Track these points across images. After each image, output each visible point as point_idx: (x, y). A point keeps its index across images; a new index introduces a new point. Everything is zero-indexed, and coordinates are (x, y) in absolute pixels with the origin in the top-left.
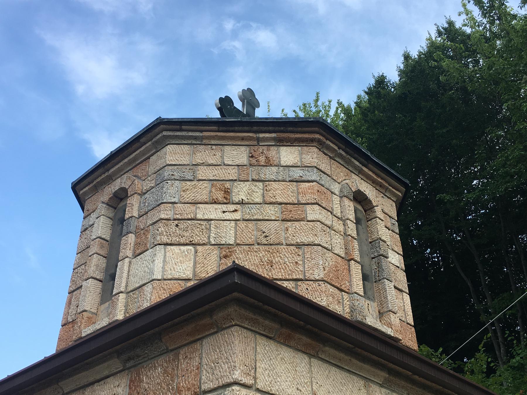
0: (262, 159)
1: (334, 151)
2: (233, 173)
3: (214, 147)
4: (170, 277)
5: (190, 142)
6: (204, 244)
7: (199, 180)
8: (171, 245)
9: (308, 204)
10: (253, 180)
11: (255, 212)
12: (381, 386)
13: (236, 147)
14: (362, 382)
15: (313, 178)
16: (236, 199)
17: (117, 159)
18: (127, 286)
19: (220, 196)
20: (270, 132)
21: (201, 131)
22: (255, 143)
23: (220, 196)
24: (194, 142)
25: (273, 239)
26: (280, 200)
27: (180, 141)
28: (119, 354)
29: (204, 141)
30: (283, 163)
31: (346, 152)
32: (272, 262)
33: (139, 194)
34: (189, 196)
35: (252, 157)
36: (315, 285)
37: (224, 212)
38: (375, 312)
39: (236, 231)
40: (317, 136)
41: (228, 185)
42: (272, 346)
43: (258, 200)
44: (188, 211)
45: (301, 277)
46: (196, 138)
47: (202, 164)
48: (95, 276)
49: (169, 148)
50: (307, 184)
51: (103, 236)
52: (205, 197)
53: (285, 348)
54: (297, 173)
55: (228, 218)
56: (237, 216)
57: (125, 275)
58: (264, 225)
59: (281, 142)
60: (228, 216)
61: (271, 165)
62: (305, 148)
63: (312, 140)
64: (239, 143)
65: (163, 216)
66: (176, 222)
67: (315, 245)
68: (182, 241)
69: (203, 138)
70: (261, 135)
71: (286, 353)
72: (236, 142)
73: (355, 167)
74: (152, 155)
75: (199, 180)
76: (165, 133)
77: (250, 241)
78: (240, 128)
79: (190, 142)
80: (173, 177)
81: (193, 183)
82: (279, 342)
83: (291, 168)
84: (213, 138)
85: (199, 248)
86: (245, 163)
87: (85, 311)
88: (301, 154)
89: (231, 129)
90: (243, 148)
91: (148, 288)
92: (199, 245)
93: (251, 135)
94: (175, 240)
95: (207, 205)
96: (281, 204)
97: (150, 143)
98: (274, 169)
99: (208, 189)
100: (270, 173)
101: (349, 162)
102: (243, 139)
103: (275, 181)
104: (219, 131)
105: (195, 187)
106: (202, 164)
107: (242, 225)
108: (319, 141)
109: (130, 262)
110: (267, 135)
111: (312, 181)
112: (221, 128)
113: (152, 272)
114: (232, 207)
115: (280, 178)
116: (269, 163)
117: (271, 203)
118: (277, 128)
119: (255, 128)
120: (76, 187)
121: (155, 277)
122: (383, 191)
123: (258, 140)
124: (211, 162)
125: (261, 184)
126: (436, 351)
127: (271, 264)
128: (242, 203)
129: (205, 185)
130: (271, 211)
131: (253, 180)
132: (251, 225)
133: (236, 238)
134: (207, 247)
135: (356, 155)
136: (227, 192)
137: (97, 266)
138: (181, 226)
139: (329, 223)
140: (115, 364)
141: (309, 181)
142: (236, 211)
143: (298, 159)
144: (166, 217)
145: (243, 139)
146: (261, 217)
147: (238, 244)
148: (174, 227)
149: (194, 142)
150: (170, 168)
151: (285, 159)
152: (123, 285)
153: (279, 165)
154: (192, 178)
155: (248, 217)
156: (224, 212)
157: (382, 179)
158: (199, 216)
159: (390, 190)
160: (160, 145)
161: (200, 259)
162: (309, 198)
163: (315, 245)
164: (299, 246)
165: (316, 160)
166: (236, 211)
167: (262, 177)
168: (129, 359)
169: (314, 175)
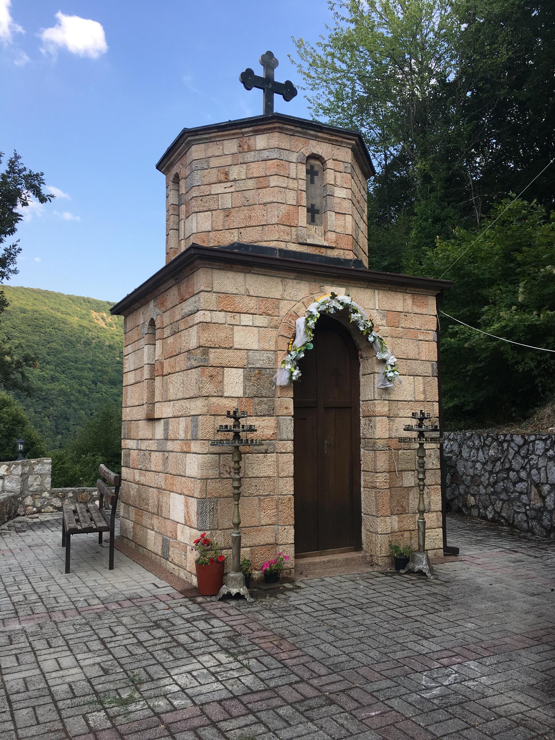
0: (246, 147)
1: (292, 130)
2: (228, 160)
3: (218, 143)
4: (200, 231)
5: (204, 141)
6: (216, 210)
7: (211, 168)
8: (200, 212)
9: (271, 175)
10: (241, 163)
11: (241, 185)
12: (295, 279)
13: (231, 140)
14: (280, 280)
15: (274, 157)
16: (231, 178)
17: (172, 152)
18: (184, 236)
19: (222, 177)
20: (248, 127)
21: (209, 133)
22: (241, 135)
23: (222, 177)
24: (207, 141)
25: (251, 202)
26: (255, 176)
27: (198, 142)
28: (172, 277)
29: (212, 140)
30: (258, 148)
31: (302, 128)
32: (250, 216)
33: (184, 178)
34: (206, 180)
35: (240, 146)
36: (272, 227)
37: (225, 188)
38: (321, 232)
39: (232, 199)
40: (277, 125)
41: (227, 169)
42: (222, 273)
43: (243, 177)
44: (205, 190)
45: (265, 223)
46: (207, 138)
47: (212, 156)
48: (173, 228)
49: (194, 148)
50: (271, 161)
51: (174, 203)
52: (214, 180)
53: (229, 272)
54: (265, 154)
55: (227, 191)
56: (232, 189)
57: (183, 230)
58: (247, 194)
59: (256, 132)
60: (228, 190)
61: (251, 151)
62: (271, 134)
63: (275, 128)
64: (232, 137)
65: (194, 195)
66: (201, 198)
67: (274, 202)
68: (205, 209)
69: (211, 138)
70: (244, 130)
71: (230, 274)
72: (231, 137)
73: (312, 135)
74: (187, 151)
75: (211, 168)
76: (189, 139)
77: (239, 205)
78: (230, 128)
79: (204, 141)
80: (197, 168)
81: (208, 171)
82: (226, 270)
83: (262, 151)
84: (217, 136)
85: (214, 212)
86: (236, 152)
87: (172, 248)
88: (268, 139)
89: (225, 129)
90: (235, 141)
91: (191, 238)
92: (214, 210)
93: (237, 131)
94: (201, 209)
95: (216, 185)
96: (256, 178)
97: (184, 144)
98: (252, 153)
99: (216, 174)
100: (250, 156)
101: (305, 134)
102: (233, 134)
103: (253, 162)
104: (219, 132)
105: (209, 173)
106: (212, 156)
107: (235, 194)
108: (279, 128)
109: (184, 222)
110: (247, 130)
111: (274, 159)
112: (220, 130)
113: (192, 229)
114: (229, 184)
115: (256, 160)
116: (249, 150)
117: (250, 178)
118: (252, 124)
119: (239, 126)
120: (157, 168)
121: (193, 232)
122: (339, 144)
123: (243, 133)
124: (217, 154)
125: (245, 165)
126: (530, 202)
127: (250, 217)
128: (235, 180)
129: (215, 171)
130: (251, 184)
131: (241, 163)
132: (240, 194)
133: (232, 204)
134: (217, 211)
135: (310, 128)
136: (227, 174)
137: (174, 222)
138: (204, 200)
139: (285, 185)
140: (171, 282)
141: (272, 159)
142: (231, 186)
143: (266, 143)
144: (196, 195)
145: (233, 134)
146: (245, 189)
147: (233, 208)
148: (200, 202)
149: (207, 141)
150: (195, 162)
151: (259, 145)
152: (183, 235)
153: (255, 150)
154: (207, 167)
155: (238, 189)
156: (225, 188)
157: (336, 136)
158: (213, 193)
159: (344, 142)
160: (189, 145)
161: (214, 219)
162: (273, 171)
163: (274, 202)
164: (265, 204)
165: (277, 143)
166: (231, 186)
167: (246, 160)
168: (176, 279)
169: (274, 154)
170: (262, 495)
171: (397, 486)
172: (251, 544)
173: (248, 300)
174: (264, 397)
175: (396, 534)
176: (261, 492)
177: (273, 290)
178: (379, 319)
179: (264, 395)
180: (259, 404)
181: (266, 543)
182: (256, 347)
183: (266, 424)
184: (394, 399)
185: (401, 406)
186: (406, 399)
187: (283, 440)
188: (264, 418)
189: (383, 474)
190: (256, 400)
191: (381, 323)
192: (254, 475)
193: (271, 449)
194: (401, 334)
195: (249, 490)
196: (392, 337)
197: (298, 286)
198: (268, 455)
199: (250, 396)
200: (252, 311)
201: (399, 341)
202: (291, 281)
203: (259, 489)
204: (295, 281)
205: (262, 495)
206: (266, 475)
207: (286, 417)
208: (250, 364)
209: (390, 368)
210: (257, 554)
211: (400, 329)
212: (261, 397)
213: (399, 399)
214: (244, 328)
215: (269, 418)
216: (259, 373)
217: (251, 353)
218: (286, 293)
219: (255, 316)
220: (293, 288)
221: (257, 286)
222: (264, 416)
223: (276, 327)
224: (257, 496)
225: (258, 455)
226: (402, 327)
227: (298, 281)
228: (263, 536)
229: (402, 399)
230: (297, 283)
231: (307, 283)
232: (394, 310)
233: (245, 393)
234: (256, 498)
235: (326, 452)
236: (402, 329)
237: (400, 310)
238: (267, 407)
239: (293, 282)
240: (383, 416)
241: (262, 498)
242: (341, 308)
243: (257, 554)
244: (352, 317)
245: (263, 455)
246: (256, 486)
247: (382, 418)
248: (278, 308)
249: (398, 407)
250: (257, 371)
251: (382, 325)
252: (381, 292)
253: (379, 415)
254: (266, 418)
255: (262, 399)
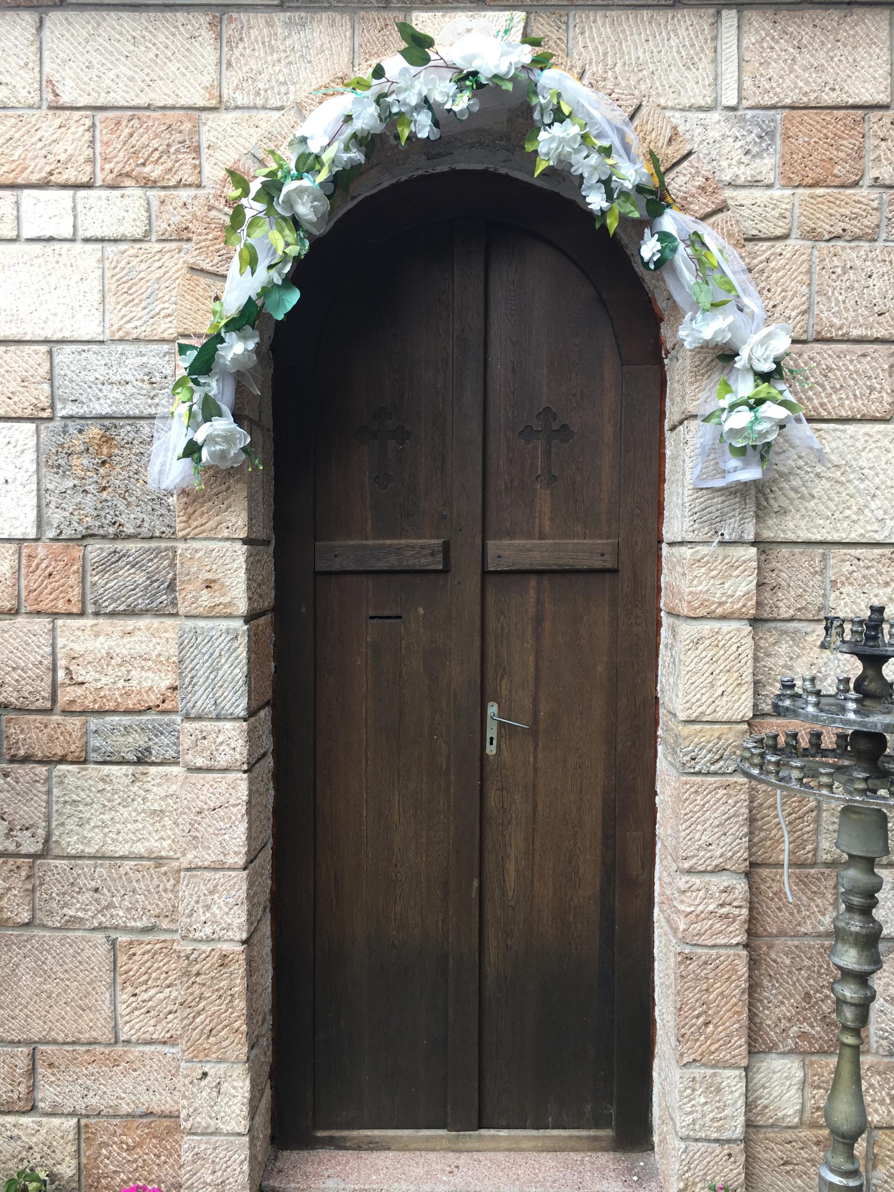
170: (126, 929)
171: (807, 928)
172: (80, 1106)
173: (49, 125)
174: (129, 537)
175: (788, 1135)
176: (120, 916)
177: (172, 67)
178: (738, 155)
179: (129, 529)
180: (108, 565)
181: (143, 1109)
182: (89, 329)
183: (141, 649)
184: (804, 535)
185: (847, 567)
186: (879, 538)
187: (199, 718)
188: (130, 623)
189: (714, 879)
190: (96, 550)
191: (744, 174)
192: (90, 850)
193: (161, 747)
194: (871, 221)
195: (66, 905)
196: (813, 236)
197: (296, 39)
198: (153, 770)
199: (68, 533)
200: (70, 175)
201: (853, 253)
202: (258, 19)
203: (110, 906)
204: (280, 17)
205: (126, 929)
206: (140, 848)
207: (210, 623)
208: (64, 401)
209: (746, 388)
210: (106, 1145)
211: (863, 193)
212: (116, 537)
213: (836, 537)
214: (37, 248)
215: (156, 622)
216: (107, 440)
217: (64, 355)
218: (231, 79)
219: (82, 193)
220: (272, 50)
221: (96, 58)
222: (131, 613)
223: (182, 235)
224: (100, 928)
225: (106, 769)
226: (876, 183)
227: (296, 15)
228: (128, 1083)
229: (854, 537)
230: (288, 24)
231: (343, 21)
232: (828, 98)
233: (40, 523)
234: (100, 937)
235: (491, 750)
236: (875, 193)
237: (866, 97)
238: (140, 578)
239: (269, 24)
240: (723, 618)
241: (123, 938)
242: (462, 103)
243: (106, 1145)
244: (542, 149)
245: (131, 769)
246: (96, 890)
247: (716, 625)
248: (197, 150)
249: (831, 574)
250: (94, 431)
251: (754, 184)
252: (756, 19)
253: (702, 612)
254: (143, 623)
255: (119, 545)
